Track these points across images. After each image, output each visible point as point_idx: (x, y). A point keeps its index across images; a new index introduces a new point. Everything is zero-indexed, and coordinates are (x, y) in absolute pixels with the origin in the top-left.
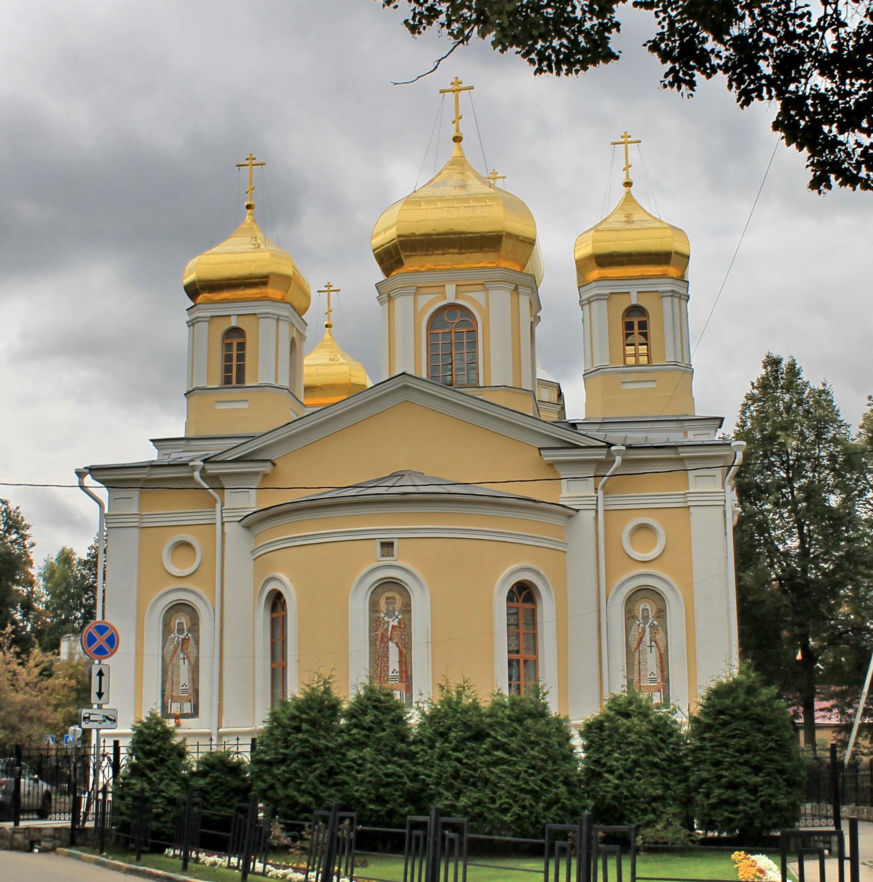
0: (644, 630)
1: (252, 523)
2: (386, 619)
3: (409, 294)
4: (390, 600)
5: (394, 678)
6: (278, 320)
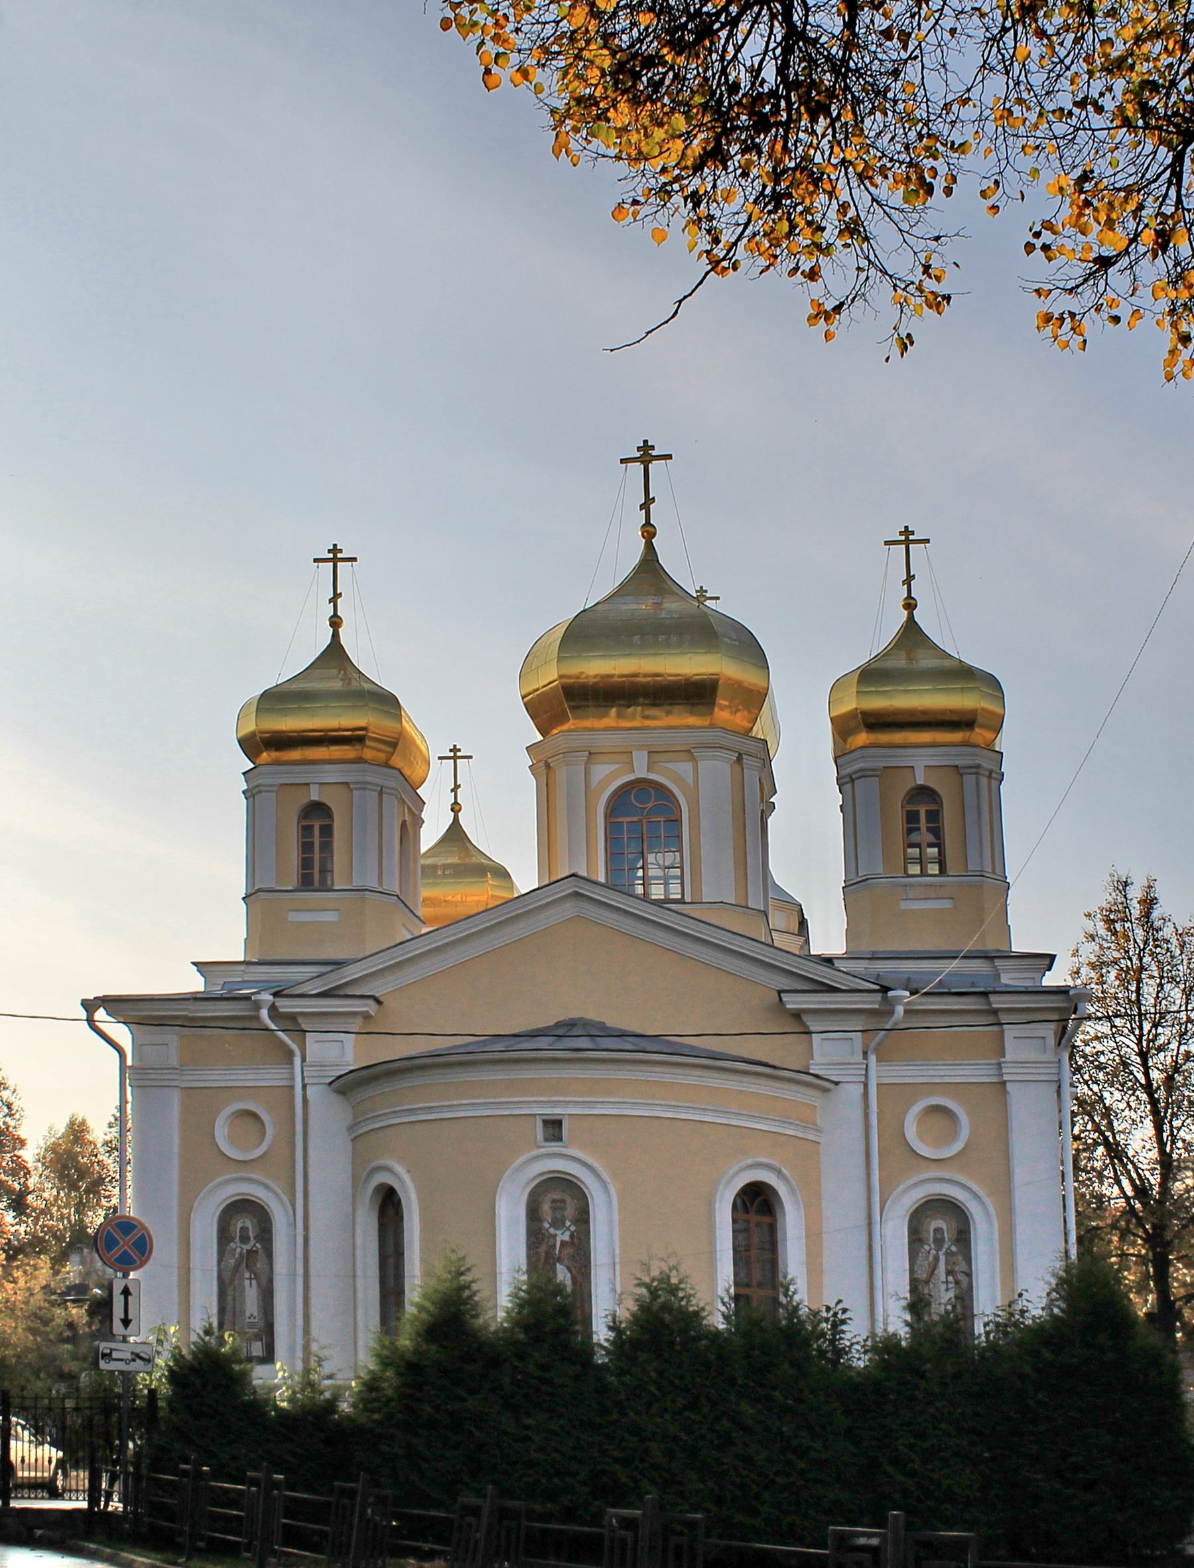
0: (937, 1259)
2: (552, 1231)
4: (558, 1205)
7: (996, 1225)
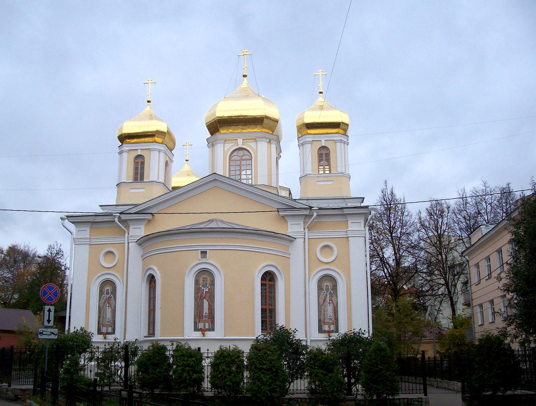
0: (326, 295)
1: (142, 242)
2: (203, 288)
3: (221, 143)
4: (205, 280)
5: (206, 317)
6: (159, 152)
7: (223, 277)
